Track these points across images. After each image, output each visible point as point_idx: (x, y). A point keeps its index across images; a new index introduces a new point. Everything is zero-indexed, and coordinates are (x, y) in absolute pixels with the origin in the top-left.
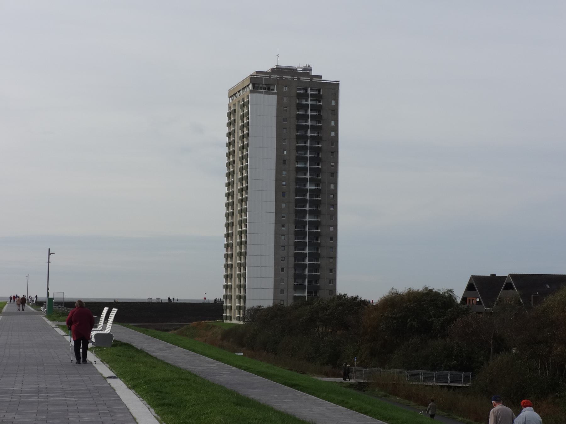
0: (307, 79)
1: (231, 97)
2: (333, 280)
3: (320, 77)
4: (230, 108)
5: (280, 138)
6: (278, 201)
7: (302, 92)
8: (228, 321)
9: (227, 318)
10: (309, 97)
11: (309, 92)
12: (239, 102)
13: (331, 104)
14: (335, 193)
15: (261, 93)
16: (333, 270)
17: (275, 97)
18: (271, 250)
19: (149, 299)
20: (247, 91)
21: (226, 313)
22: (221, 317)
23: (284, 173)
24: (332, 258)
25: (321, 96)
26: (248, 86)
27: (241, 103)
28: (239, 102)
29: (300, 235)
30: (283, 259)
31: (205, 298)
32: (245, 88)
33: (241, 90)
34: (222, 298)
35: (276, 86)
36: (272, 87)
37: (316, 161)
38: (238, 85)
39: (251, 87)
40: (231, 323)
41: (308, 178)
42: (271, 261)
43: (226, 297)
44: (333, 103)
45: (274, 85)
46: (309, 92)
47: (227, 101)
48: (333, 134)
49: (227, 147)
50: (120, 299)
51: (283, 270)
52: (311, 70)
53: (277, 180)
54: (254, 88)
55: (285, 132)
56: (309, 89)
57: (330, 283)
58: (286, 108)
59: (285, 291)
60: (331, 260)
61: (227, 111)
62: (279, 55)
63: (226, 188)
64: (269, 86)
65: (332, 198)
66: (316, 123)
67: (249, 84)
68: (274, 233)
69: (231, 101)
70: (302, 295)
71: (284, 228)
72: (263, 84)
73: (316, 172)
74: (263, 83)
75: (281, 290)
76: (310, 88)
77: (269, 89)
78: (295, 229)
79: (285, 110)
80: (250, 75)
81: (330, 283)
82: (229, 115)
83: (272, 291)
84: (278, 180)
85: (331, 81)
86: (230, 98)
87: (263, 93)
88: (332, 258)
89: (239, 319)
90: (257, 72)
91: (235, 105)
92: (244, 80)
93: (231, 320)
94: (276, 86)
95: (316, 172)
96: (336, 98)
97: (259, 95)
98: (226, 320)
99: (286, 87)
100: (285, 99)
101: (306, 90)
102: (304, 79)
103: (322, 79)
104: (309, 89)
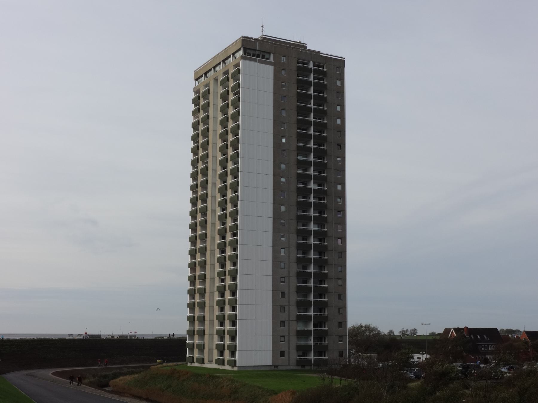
2: (343, 309)
5: (278, 121)
6: (276, 203)
8: (196, 365)
10: (311, 73)
11: (311, 66)
13: (336, 84)
14: (342, 196)
15: (255, 60)
16: (342, 295)
17: (271, 68)
18: (268, 268)
19: (70, 335)
22: (183, 358)
23: (283, 166)
24: (340, 279)
25: (324, 73)
27: (221, 78)
29: (304, 248)
30: (283, 279)
31: (86, 333)
33: (230, 56)
34: (185, 333)
35: (272, 54)
36: (267, 56)
37: (320, 154)
38: (205, 65)
39: (241, 53)
40: (203, 367)
41: (312, 175)
42: (268, 283)
43: (191, 333)
44: (338, 83)
45: (270, 53)
46: (311, 66)
47: (193, 84)
48: (339, 122)
49: (192, 140)
50: (146, 335)
51: (283, 295)
53: (275, 175)
54: (245, 54)
55: (283, 113)
56: (311, 63)
57: (339, 312)
58: (285, 84)
59: (286, 323)
60: (340, 282)
61: (193, 96)
62: (264, 27)
63: (191, 191)
64: (264, 54)
65: (339, 202)
67: (240, 49)
68: (272, 245)
69: (197, 84)
71: (284, 239)
72: (256, 50)
73: (320, 167)
74: (258, 49)
75: (281, 322)
76: (313, 62)
77: (263, 57)
79: (283, 86)
80: (241, 36)
81: (339, 312)
83: (270, 324)
84: (276, 175)
85: (332, 56)
86: (197, 81)
87: (257, 62)
92: (227, 47)
93: (203, 363)
94: (272, 54)
95: (320, 167)
96: (219, 150)
97: (253, 63)
99: (284, 58)
100: (283, 72)
104: (311, 63)
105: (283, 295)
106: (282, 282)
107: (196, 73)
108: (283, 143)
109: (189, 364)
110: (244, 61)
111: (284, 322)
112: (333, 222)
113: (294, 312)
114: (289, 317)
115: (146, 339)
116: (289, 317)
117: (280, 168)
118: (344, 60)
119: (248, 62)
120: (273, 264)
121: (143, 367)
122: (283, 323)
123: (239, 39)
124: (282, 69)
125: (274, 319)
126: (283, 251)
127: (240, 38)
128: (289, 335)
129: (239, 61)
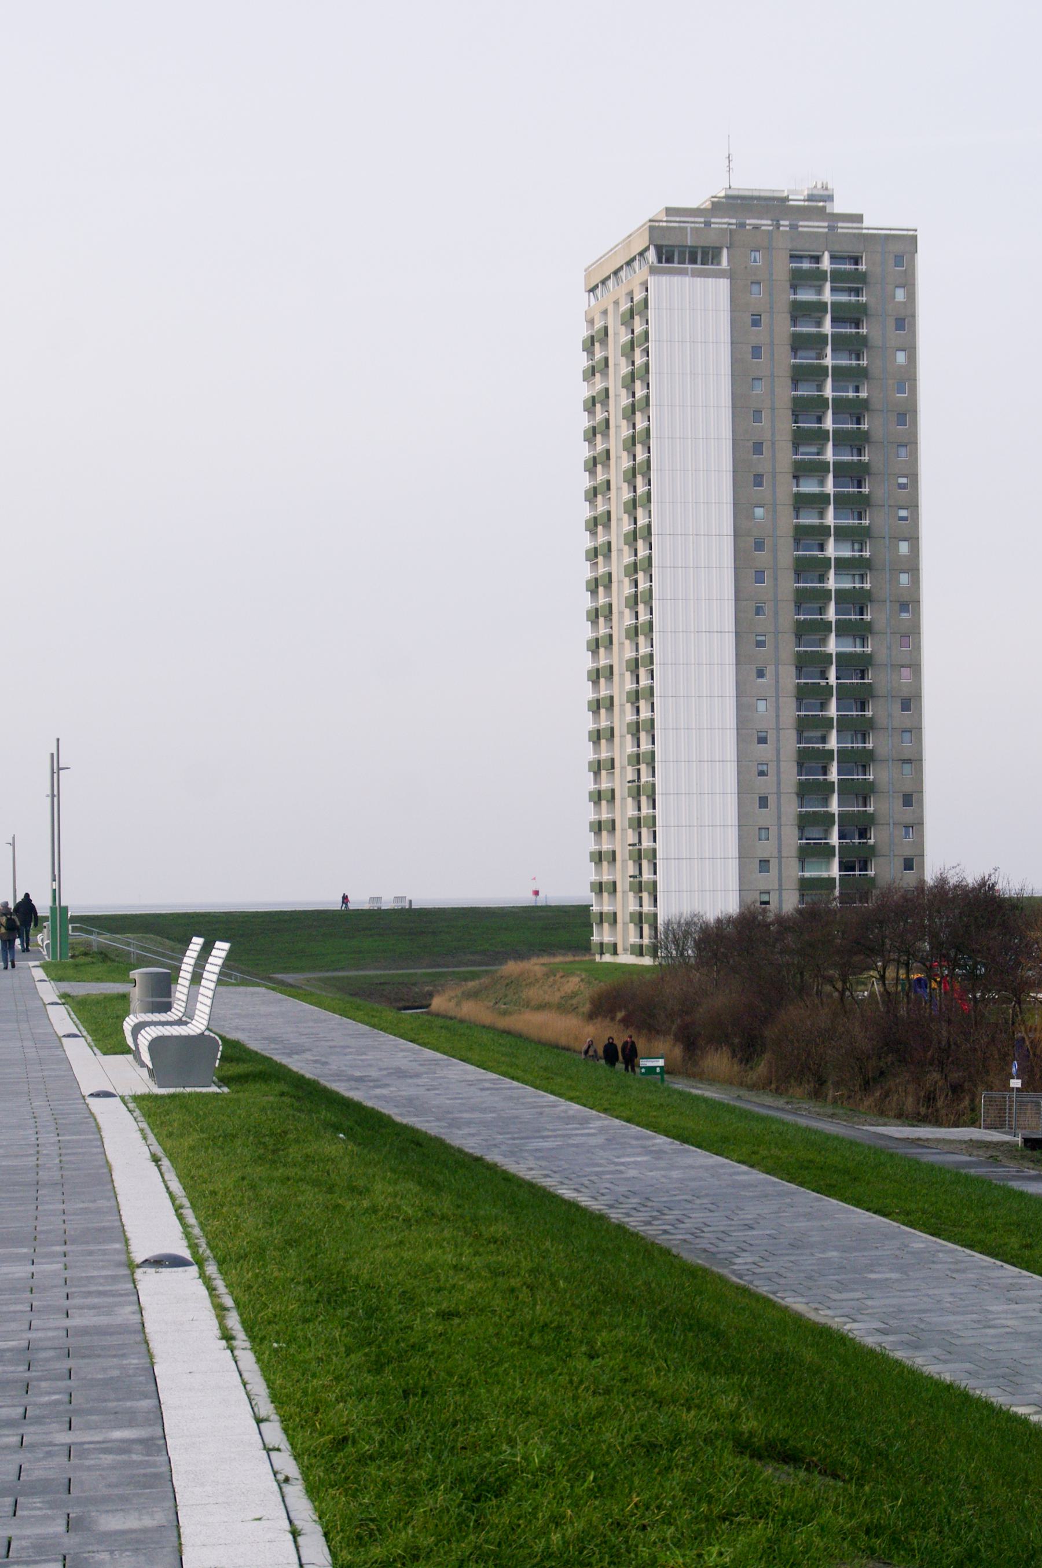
0: (819, 226)
1: (592, 290)
3: (859, 218)
4: (591, 322)
7: (806, 265)
8: (607, 958)
9: (602, 948)
11: (826, 264)
12: (616, 303)
13: (894, 298)
17: (723, 285)
20: (640, 271)
21: (601, 934)
22: (585, 947)
23: (759, 512)
24: (909, 761)
26: (641, 254)
27: (625, 306)
28: (616, 303)
32: (633, 260)
35: (725, 252)
38: (600, 262)
39: (651, 255)
44: (900, 295)
46: (826, 264)
47: (583, 301)
51: (763, 802)
52: (830, 198)
56: (826, 256)
59: (773, 865)
62: (733, 157)
66: (851, 360)
67: (647, 249)
70: (825, 874)
76: (830, 252)
78: (800, 774)
80: (647, 219)
82: (589, 345)
83: (732, 867)
88: (909, 761)
89: (639, 951)
90: (669, 211)
91: (605, 312)
92: (630, 236)
93: (615, 953)
97: (676, 280)
98: (602, 953)
101: (817, 259)
102: (807, 226)
103: (865, 224)
104: (826, 256)
105: (763, 802)
106: (762, 773)
107: (588, 272)
108: (900, 366)
109: (597, 958)
110: (656, 277)
111: (769, 861)
112: (888, 630)
113: (792, 840)
114: (780, 851)
115: (384, 910)
116: (780, 851)
117: (751, 516)
118: (916, 233)
119: (664, 279)
120: (738, 734)
121: (86, 929)
122: (764, 864)
123: (643, 226)
124: (752, 283)
125: (743, 856)
126: (761, 706)
127: (645, 224)
128: (780, 890)
129: (645, 278)
